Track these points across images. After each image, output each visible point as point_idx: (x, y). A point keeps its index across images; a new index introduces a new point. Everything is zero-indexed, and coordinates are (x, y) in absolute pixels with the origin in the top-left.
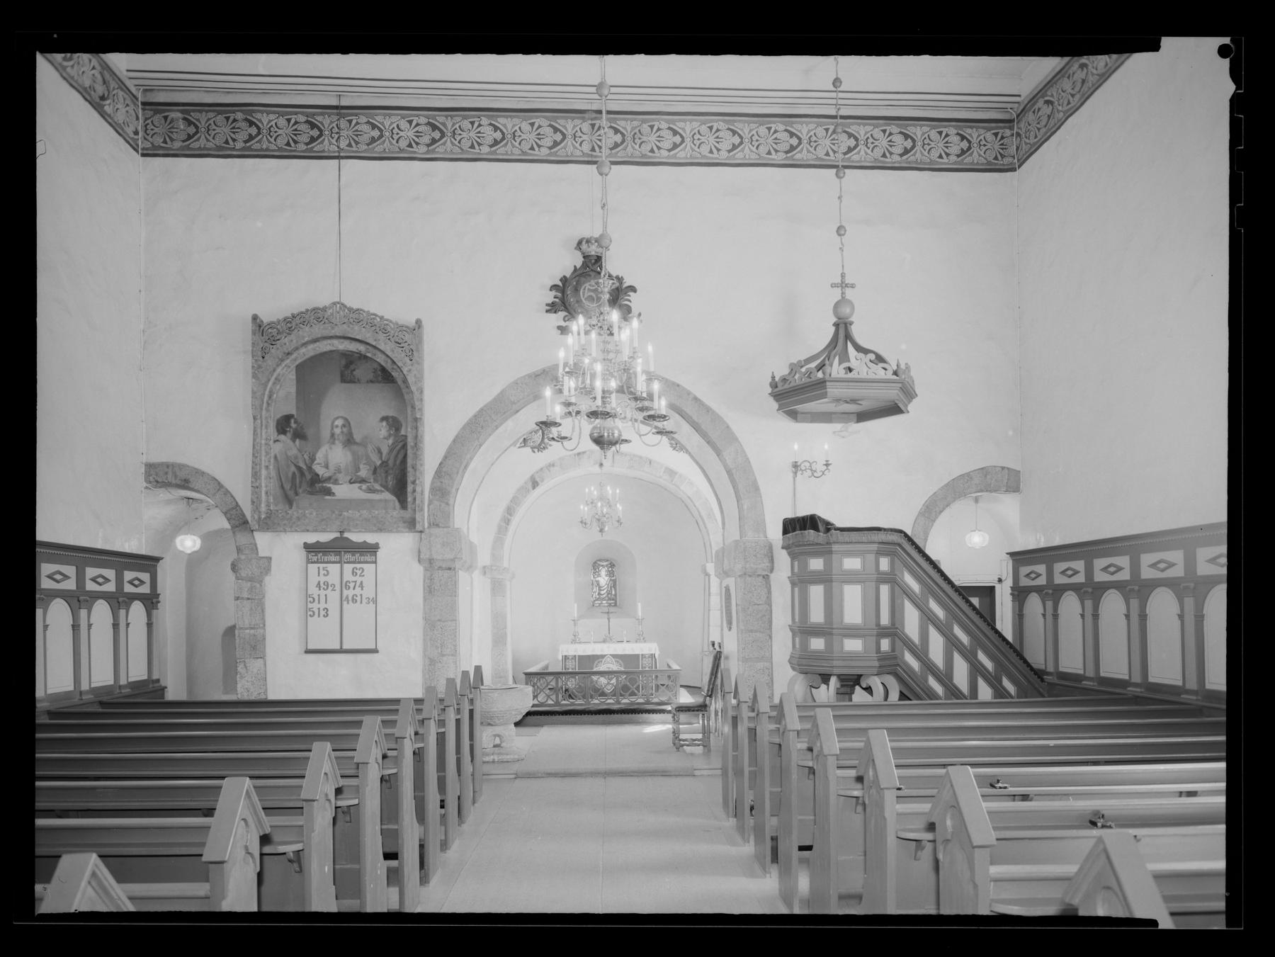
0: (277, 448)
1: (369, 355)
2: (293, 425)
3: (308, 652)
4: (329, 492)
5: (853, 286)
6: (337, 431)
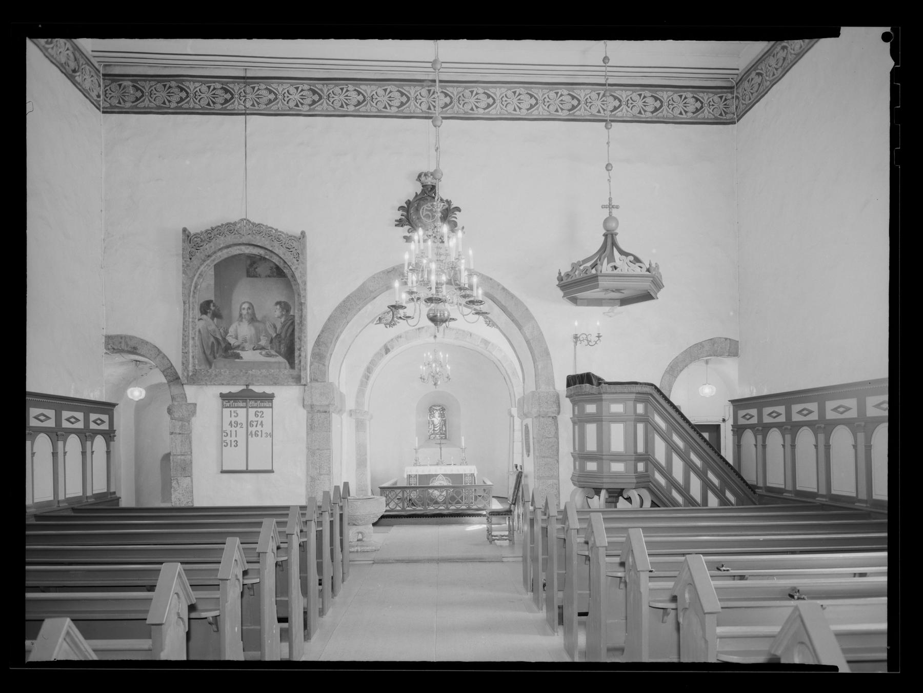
0: (200, 325)
1: (267, 257)
2: (212, 308)
3: (223, 472)
4: (238, 356)
5: (617, 207)
6: (244, 312)
